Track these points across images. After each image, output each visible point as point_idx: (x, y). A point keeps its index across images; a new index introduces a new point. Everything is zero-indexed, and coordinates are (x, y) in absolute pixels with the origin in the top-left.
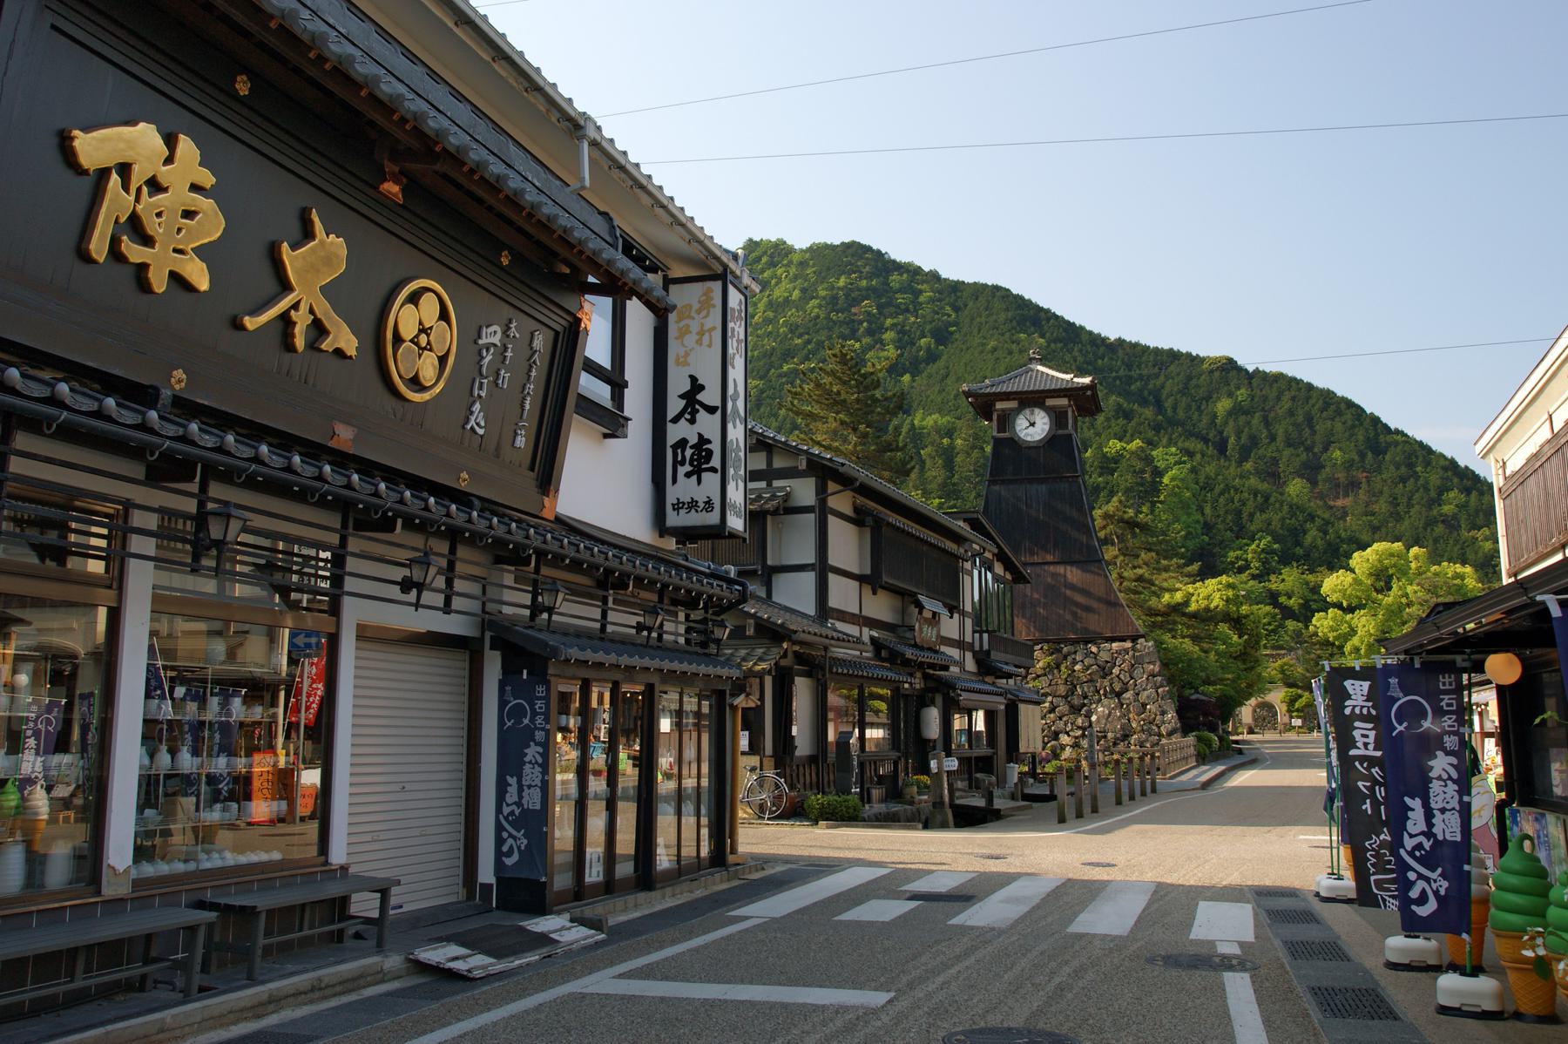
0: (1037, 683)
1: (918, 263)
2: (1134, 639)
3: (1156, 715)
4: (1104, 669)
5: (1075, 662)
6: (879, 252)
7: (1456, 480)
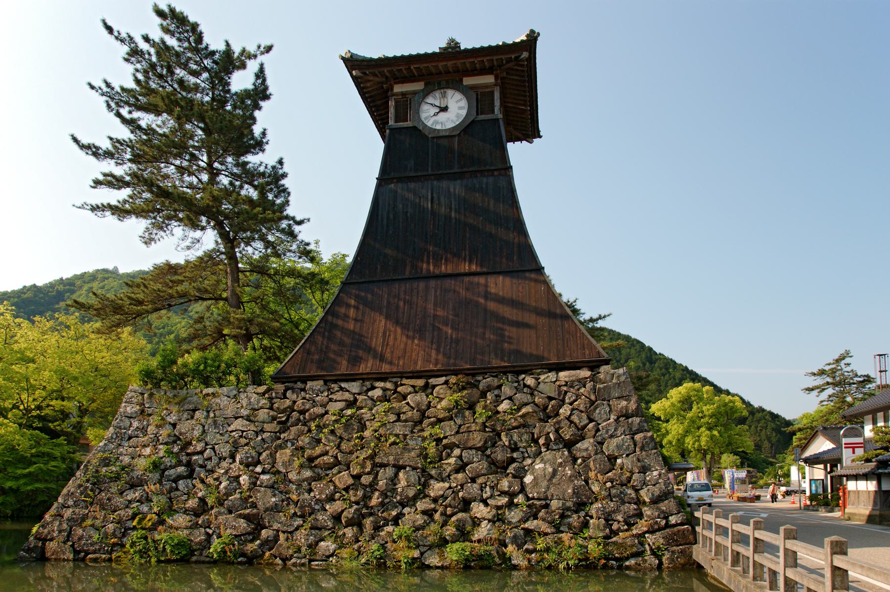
0: (437, 430)
2: (594, 366)
3: (632, 473)
4: (546, 408)
5: (498, 400)
7: (688, 375)
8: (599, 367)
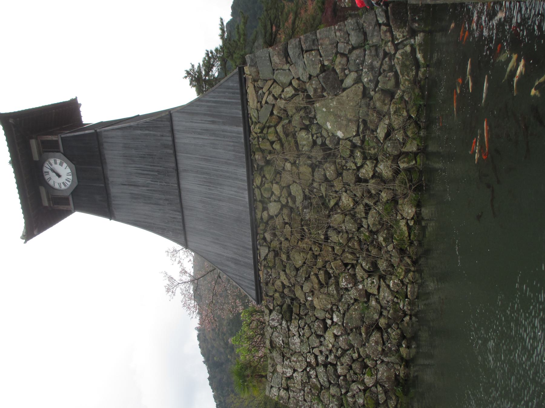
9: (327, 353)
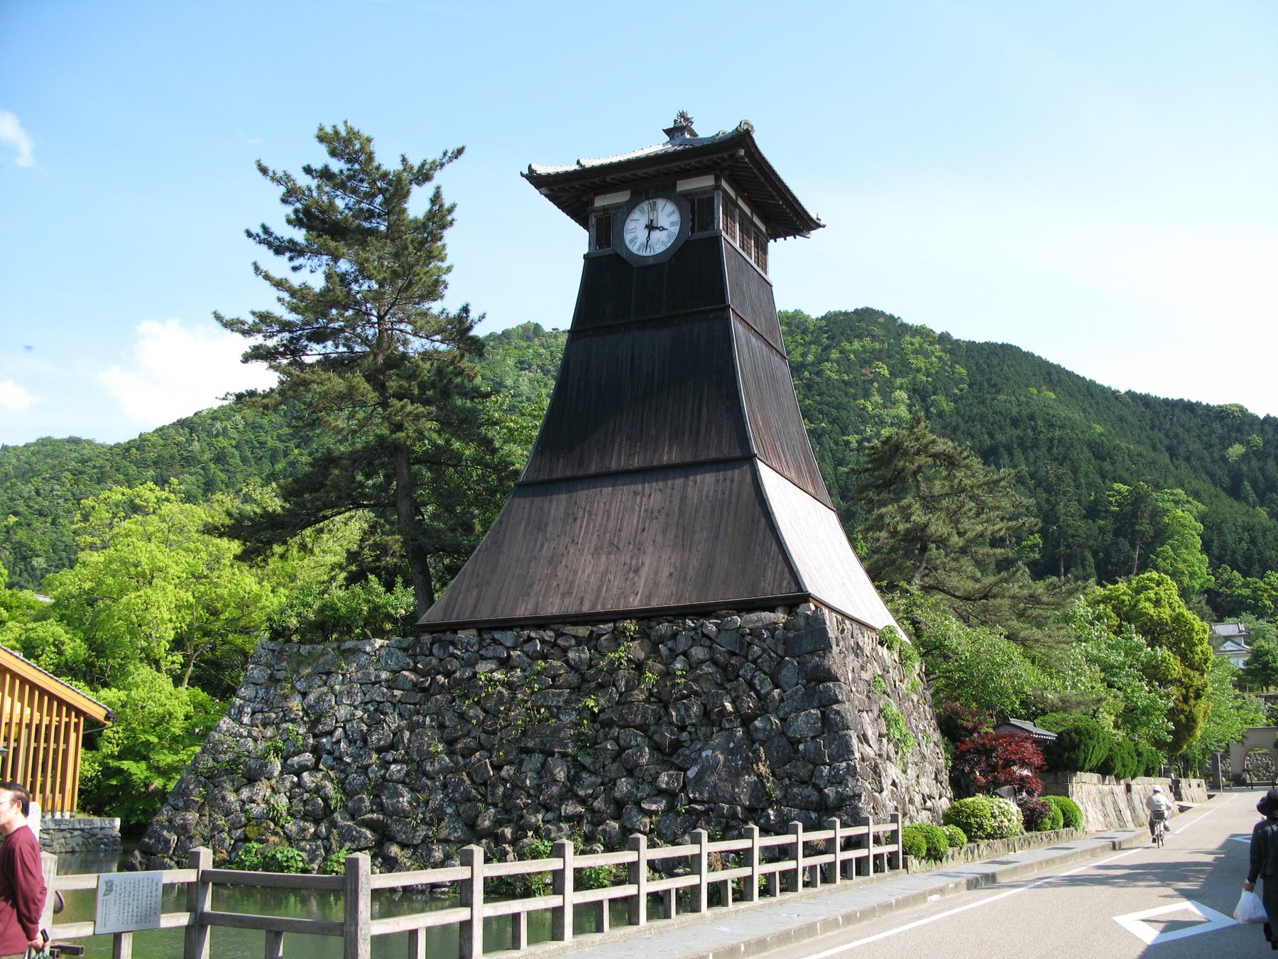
1: (929, 326)
6: (891, 317)
8: (797, 605)
9: (337, 754)
